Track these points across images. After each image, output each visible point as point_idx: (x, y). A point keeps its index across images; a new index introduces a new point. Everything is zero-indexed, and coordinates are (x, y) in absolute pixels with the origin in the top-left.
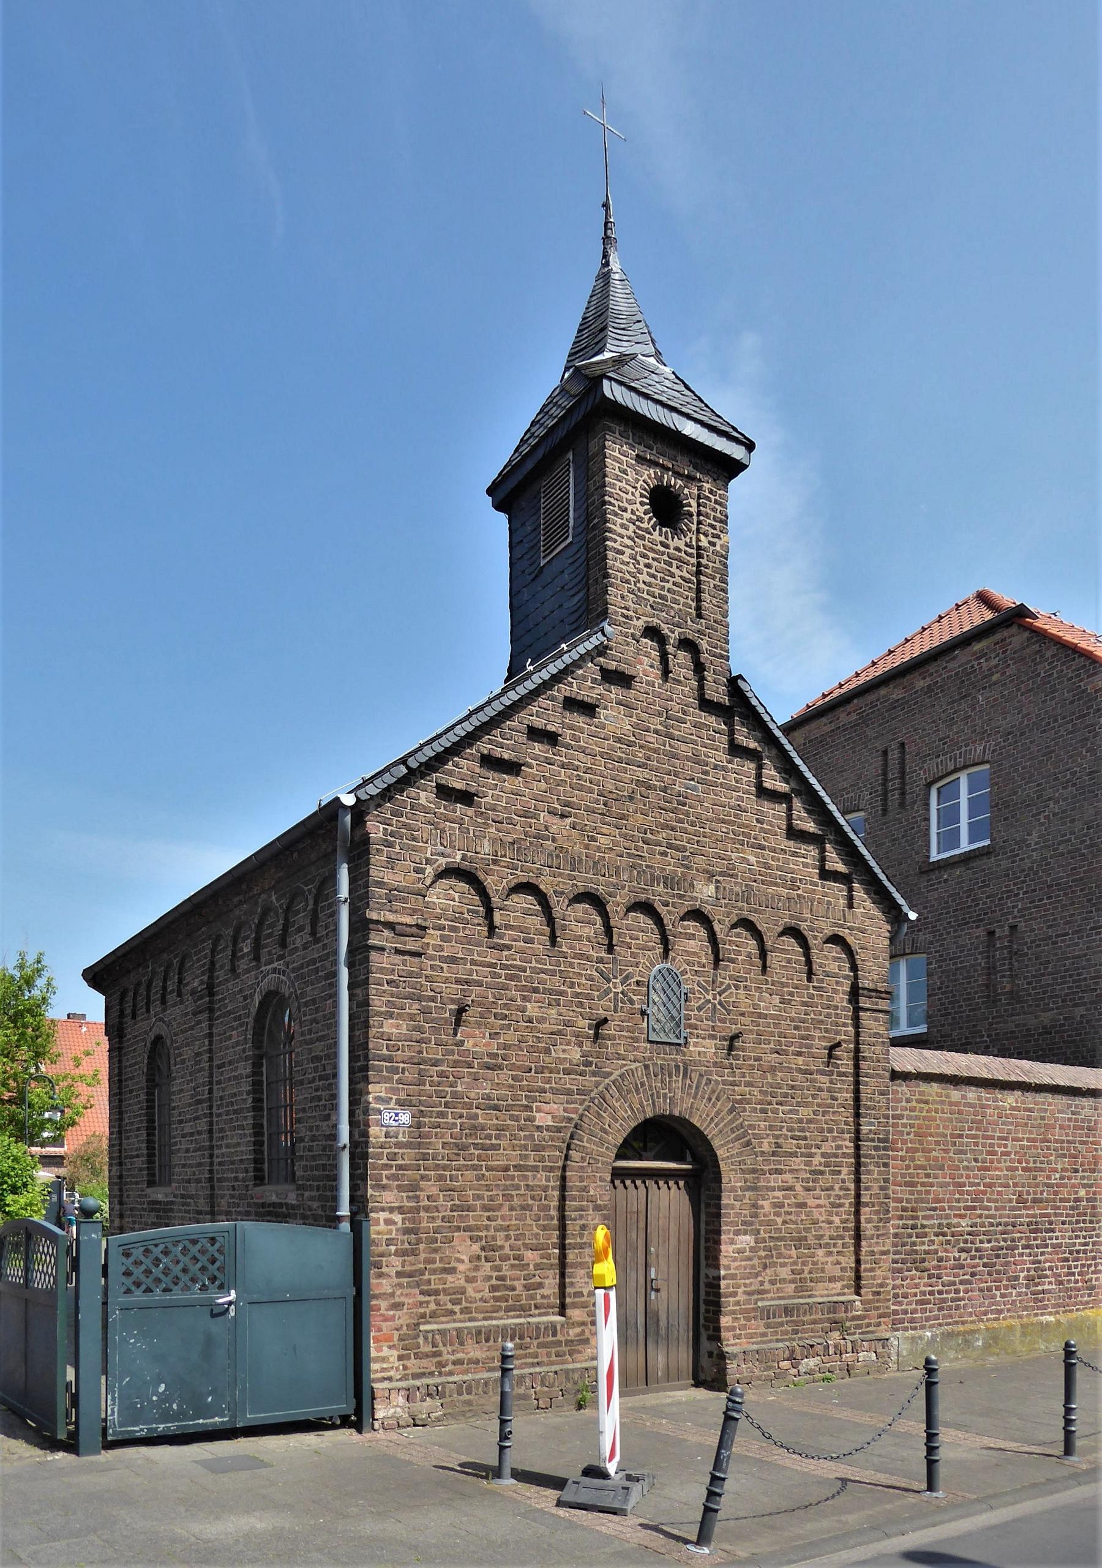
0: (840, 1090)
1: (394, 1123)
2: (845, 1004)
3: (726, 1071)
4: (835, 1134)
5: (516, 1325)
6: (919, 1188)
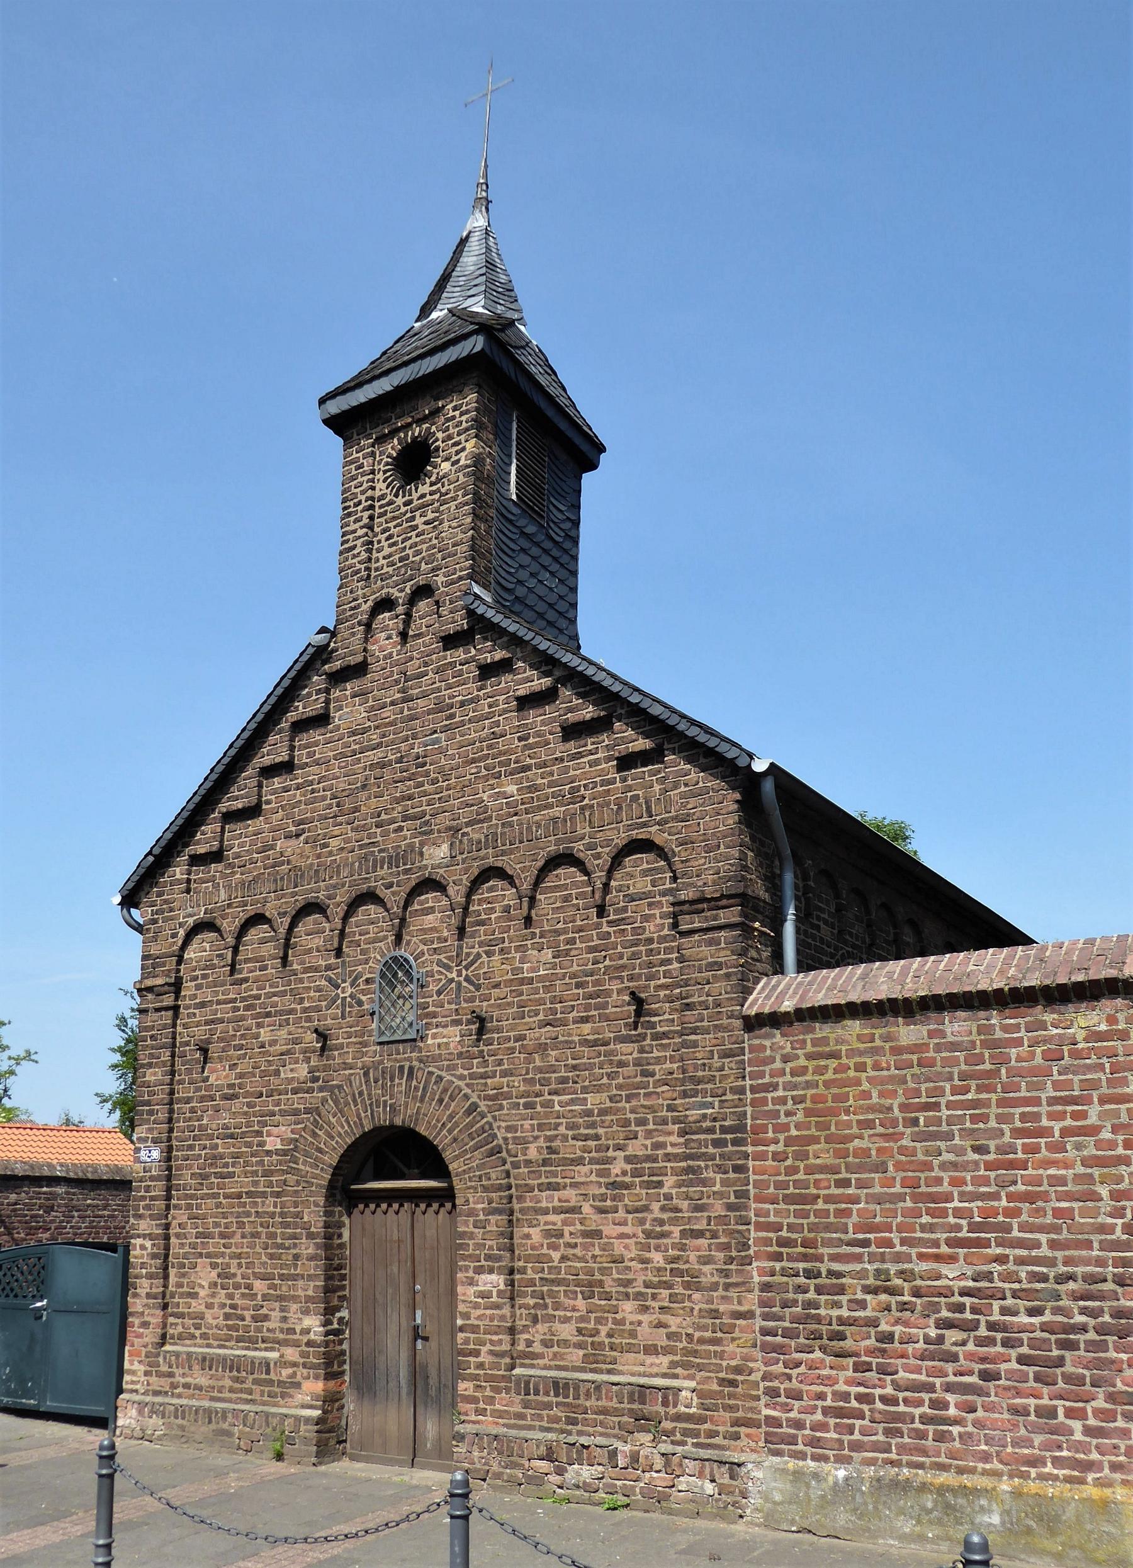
0: (659, 1061)
1: (149, 1160)
2: (666, 932)
3: (475, 1061)
4: (651, 1126)
5: (235, 1356)
6: (820, 1205)
